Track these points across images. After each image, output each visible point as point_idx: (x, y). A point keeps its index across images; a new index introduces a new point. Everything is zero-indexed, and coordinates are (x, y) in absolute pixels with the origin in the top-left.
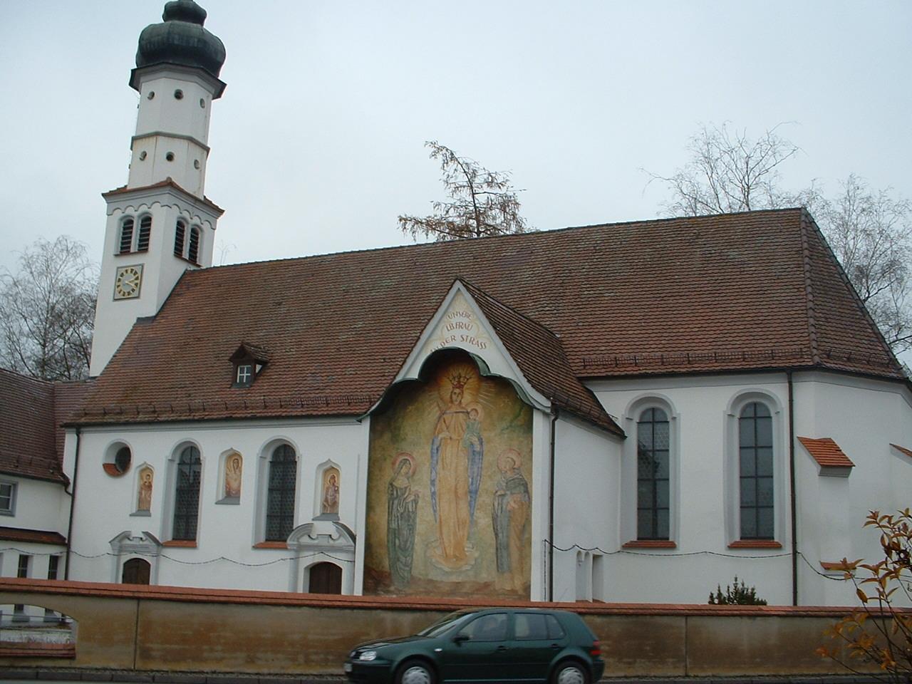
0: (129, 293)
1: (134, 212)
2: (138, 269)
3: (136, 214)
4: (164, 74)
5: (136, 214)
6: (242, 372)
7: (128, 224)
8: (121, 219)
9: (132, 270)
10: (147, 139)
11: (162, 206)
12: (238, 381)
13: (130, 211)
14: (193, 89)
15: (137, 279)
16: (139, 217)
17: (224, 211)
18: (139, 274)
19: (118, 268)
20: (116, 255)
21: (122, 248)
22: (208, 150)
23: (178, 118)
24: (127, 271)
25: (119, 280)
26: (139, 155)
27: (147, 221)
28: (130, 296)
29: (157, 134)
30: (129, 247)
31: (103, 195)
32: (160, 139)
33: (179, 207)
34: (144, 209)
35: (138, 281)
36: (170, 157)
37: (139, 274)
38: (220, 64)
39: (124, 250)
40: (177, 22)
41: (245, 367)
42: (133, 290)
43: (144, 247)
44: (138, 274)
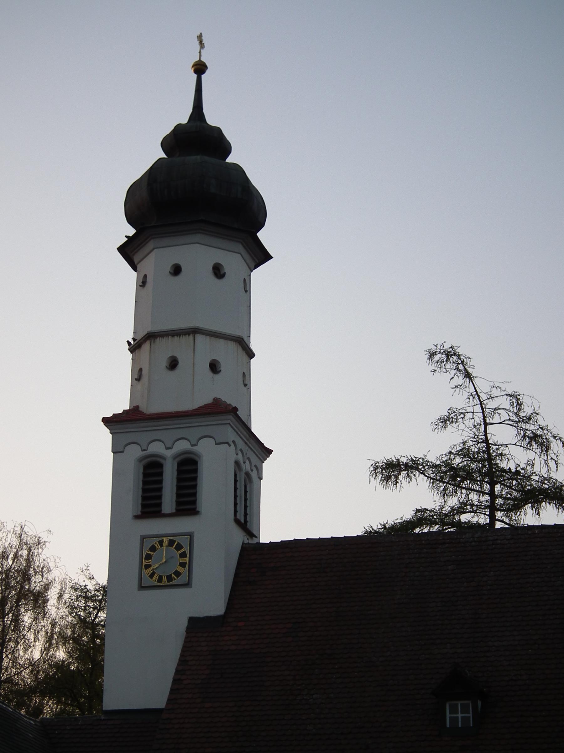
0: (170, 578)
1: (167, 447)
2: (184, 541)
3: (168, 454)
4: (198, 237)
5: (168, 454)
6: (454, 710)
7: (151, 470)
8: (141, 460)
9: (171, 543)
10: (176, 338)
11: (217, 444)
12: (448, 725)
13: (157, 448)
14: (232, 261)
15: (183, 555)
16: (175, 457)
17: (272, 451)
18: (186, 549)
19: (143, 538)
20: (137, 517)
21: (143, 506)
22: (251, 355)
23: (196, 302)
24: (161, 543)
25: (148, 557)
26: (164, 363)
27: (188, 467)
28: (170, 583)
29: (194, 331)
30: (160, 505)
31: (106, 421)
32: (200, 338)
33: (163, 442)
34: (182, 446)
35: (186, 560)
36: (214, 367)
37: (186, 549)
38: (261, 225)
39: (149, 507)
40: (206, 158)
41: (459, 703)
42: (178, 574)
43: (187, 505)
44: (183, 548)
